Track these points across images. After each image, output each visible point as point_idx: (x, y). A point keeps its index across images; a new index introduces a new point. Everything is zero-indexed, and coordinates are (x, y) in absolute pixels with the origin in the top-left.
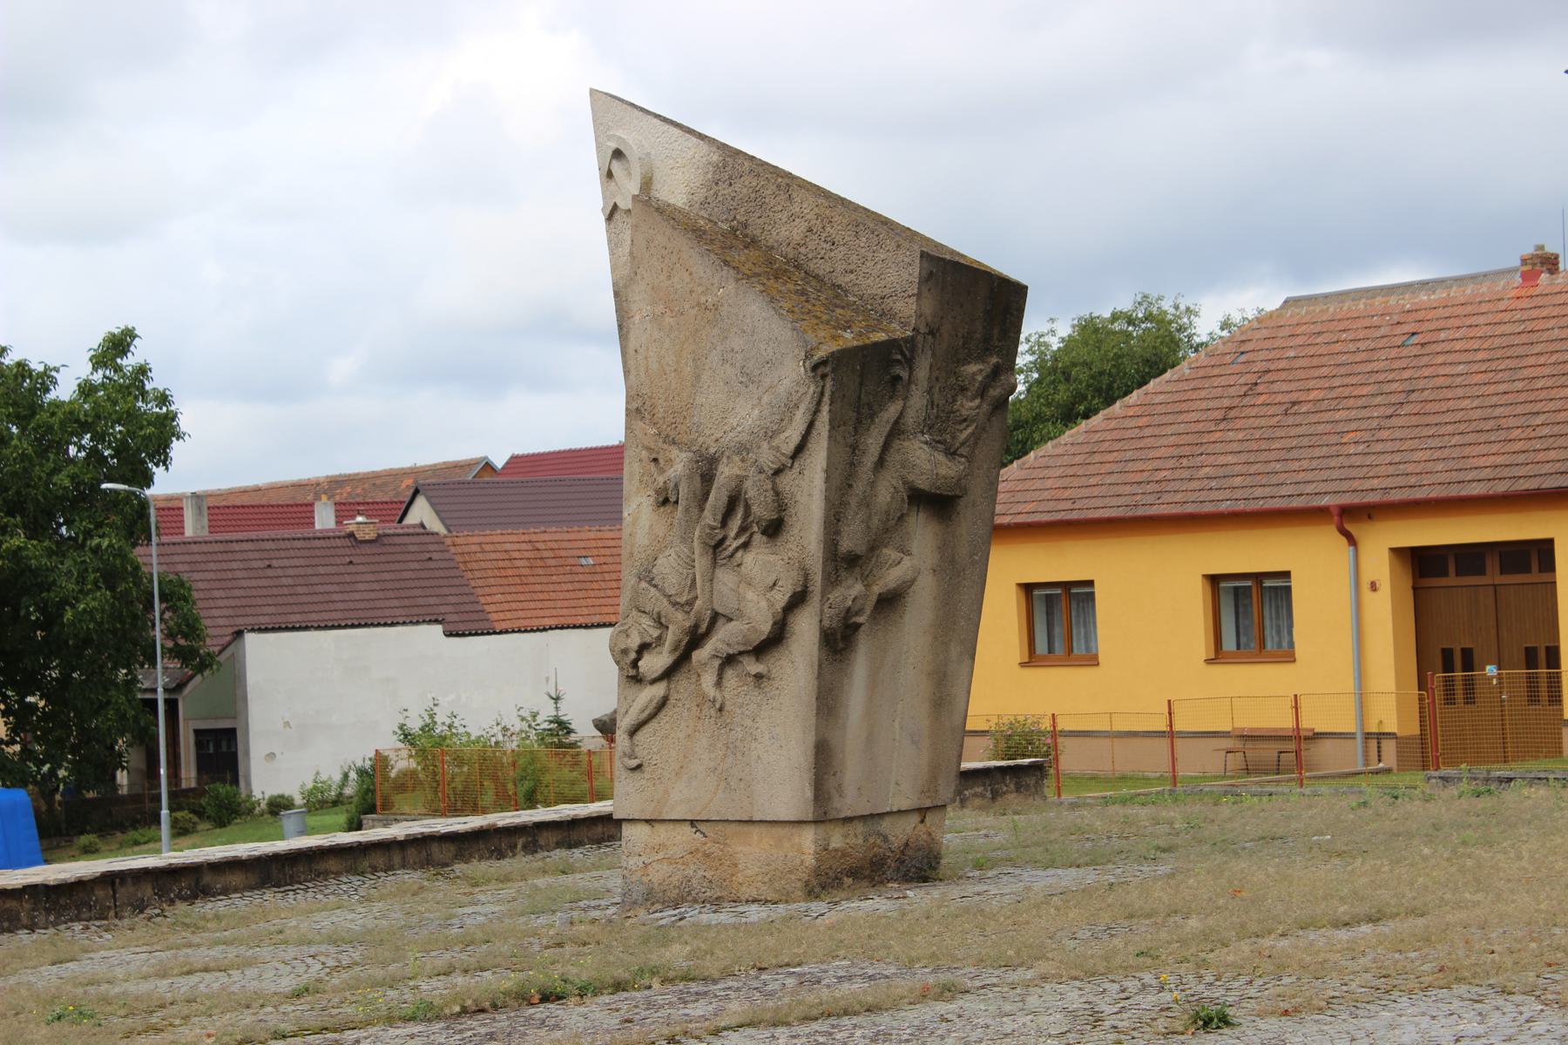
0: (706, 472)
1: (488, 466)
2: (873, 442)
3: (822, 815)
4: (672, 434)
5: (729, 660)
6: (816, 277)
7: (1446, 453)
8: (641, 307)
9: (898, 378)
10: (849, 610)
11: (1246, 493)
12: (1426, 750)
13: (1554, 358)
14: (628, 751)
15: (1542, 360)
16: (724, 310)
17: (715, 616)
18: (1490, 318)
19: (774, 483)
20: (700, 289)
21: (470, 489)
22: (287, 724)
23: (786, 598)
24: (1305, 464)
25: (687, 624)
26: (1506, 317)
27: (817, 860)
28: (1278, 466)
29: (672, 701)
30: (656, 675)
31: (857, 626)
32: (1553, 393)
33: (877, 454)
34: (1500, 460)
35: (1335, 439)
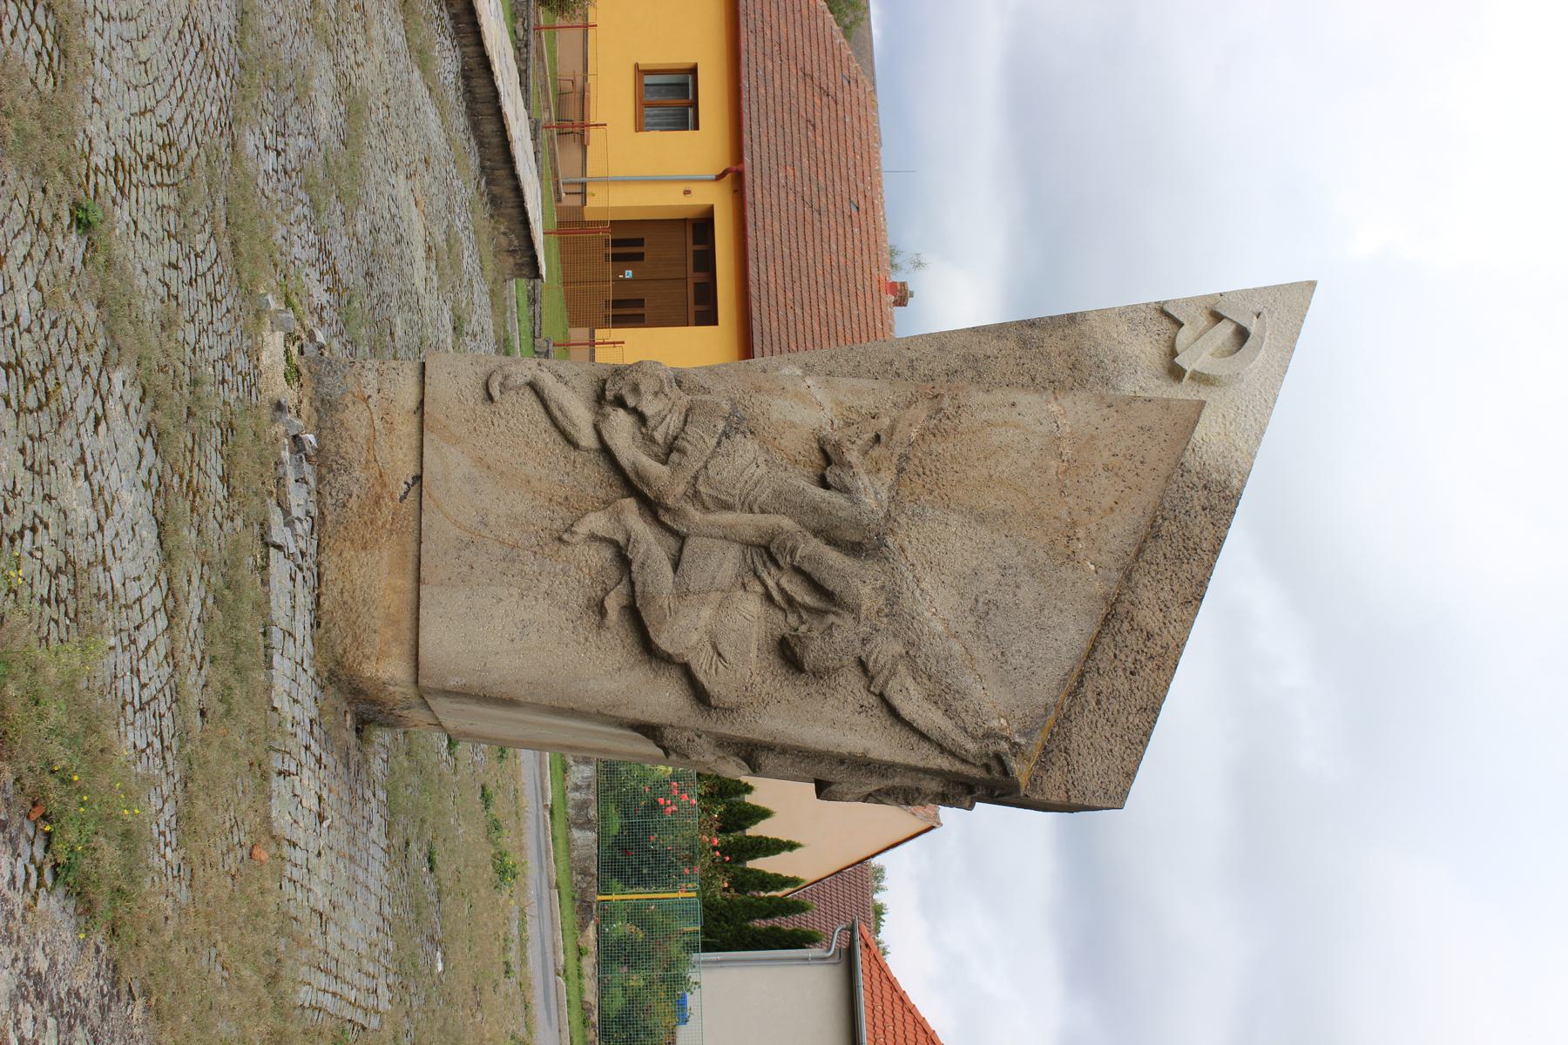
0: (862, 545)
5: (623, 560)
7: (778, 245)
11: (753, 99)
16: (1067, 573)
18: (866, 263)
20: (1093, 527)
24: (772, 141)
26: (867, 275)
28: (771, 120)
29: (573, 454)
30: (606, 437)
32: (815, 318)
34: (772, 286)
35: (789, 160)
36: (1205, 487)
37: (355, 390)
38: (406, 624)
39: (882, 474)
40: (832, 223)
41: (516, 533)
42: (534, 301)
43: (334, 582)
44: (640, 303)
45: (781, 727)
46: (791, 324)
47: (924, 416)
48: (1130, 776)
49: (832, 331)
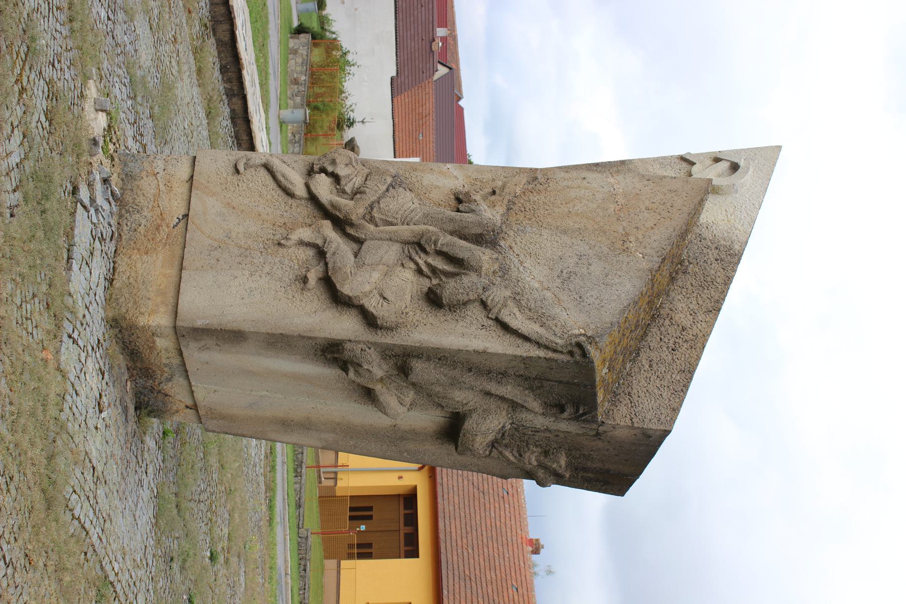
0: (485, 238)
1: (459, 99)
2: (508, 390)
3: (183, 334)
4: (516, 208)
5: (321, 254)
6: (645, 334)
7: (457, 510)
8: (621, 183)
9: (562, 409)
10: (360, 365)
12: (328, 499)
13: (496, 555)
14: (251, 163)
15: (496, 550)
16: (623, 258)
17: (359, 242)
18: (514, 526)
19: (474, 301)
20: (640, 236)
21: (450, 91)
22: (356, 9)
23: (371, 309)
25: (354, 217)
26: (514, 533)
27: (143, 327)
29: (290, 201)
31: (345, 370)
32: (481, 556)
33: (498, 393)
34: (454, 534)
36: (717, 248)
37: (149, 169)
38: (171, 294)
39: (497, 208)
40: (492, 500)
41: (249, 242)
42: (300, 506)
43: (124, 272)
44: (370, 545)
45: (426, 338)
46: (466, 559)
47: (524, 181)
48: (676, 410)
49: (492, 566)
